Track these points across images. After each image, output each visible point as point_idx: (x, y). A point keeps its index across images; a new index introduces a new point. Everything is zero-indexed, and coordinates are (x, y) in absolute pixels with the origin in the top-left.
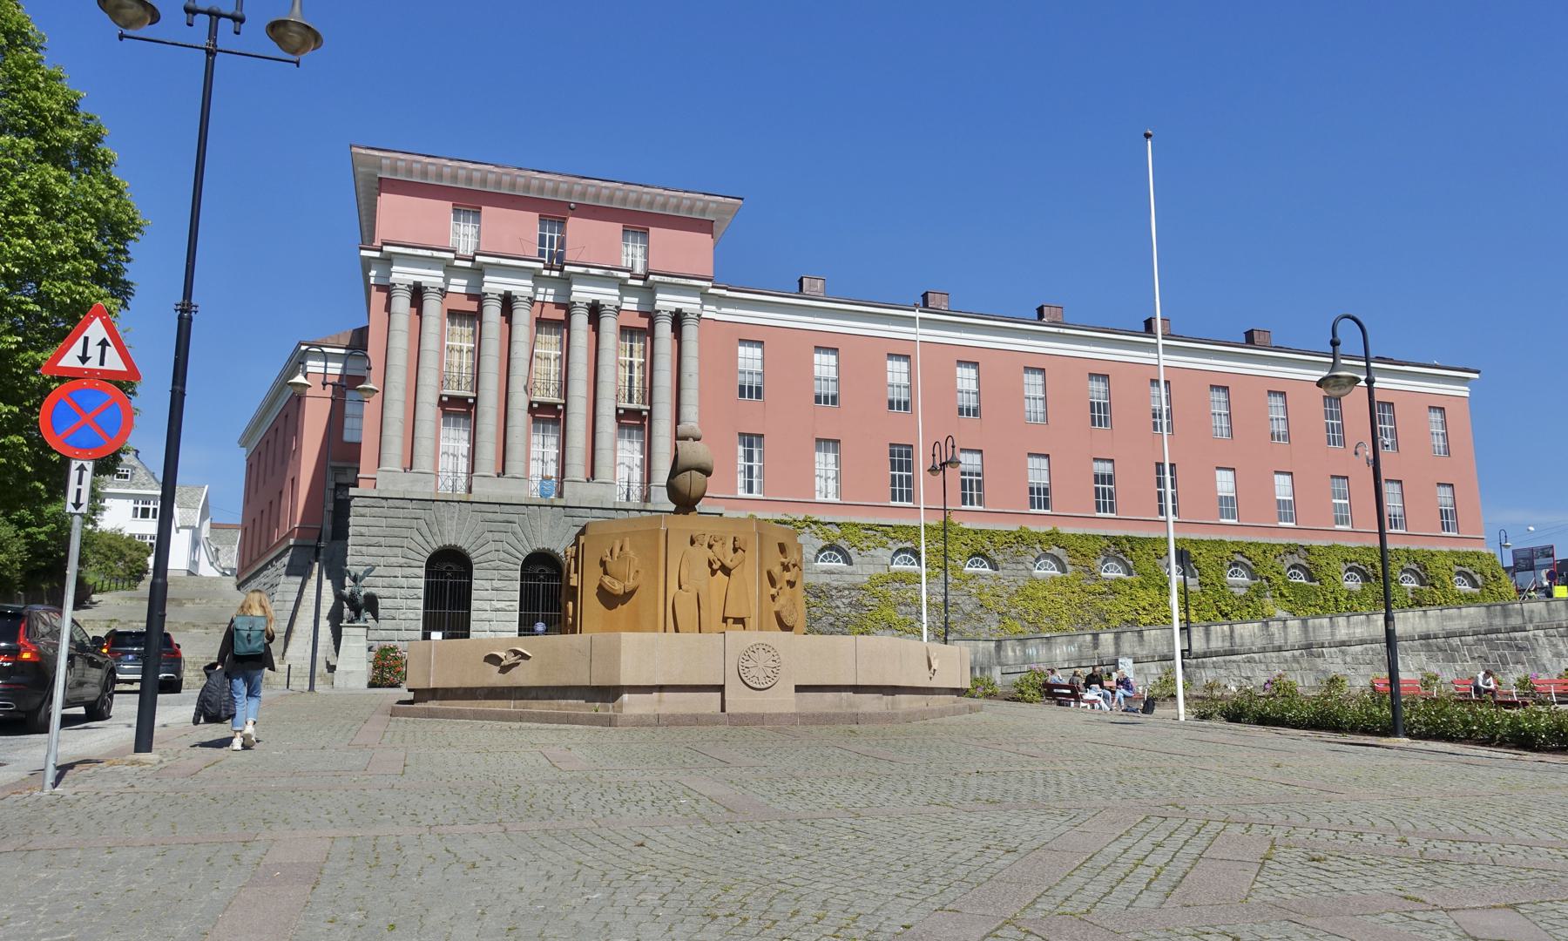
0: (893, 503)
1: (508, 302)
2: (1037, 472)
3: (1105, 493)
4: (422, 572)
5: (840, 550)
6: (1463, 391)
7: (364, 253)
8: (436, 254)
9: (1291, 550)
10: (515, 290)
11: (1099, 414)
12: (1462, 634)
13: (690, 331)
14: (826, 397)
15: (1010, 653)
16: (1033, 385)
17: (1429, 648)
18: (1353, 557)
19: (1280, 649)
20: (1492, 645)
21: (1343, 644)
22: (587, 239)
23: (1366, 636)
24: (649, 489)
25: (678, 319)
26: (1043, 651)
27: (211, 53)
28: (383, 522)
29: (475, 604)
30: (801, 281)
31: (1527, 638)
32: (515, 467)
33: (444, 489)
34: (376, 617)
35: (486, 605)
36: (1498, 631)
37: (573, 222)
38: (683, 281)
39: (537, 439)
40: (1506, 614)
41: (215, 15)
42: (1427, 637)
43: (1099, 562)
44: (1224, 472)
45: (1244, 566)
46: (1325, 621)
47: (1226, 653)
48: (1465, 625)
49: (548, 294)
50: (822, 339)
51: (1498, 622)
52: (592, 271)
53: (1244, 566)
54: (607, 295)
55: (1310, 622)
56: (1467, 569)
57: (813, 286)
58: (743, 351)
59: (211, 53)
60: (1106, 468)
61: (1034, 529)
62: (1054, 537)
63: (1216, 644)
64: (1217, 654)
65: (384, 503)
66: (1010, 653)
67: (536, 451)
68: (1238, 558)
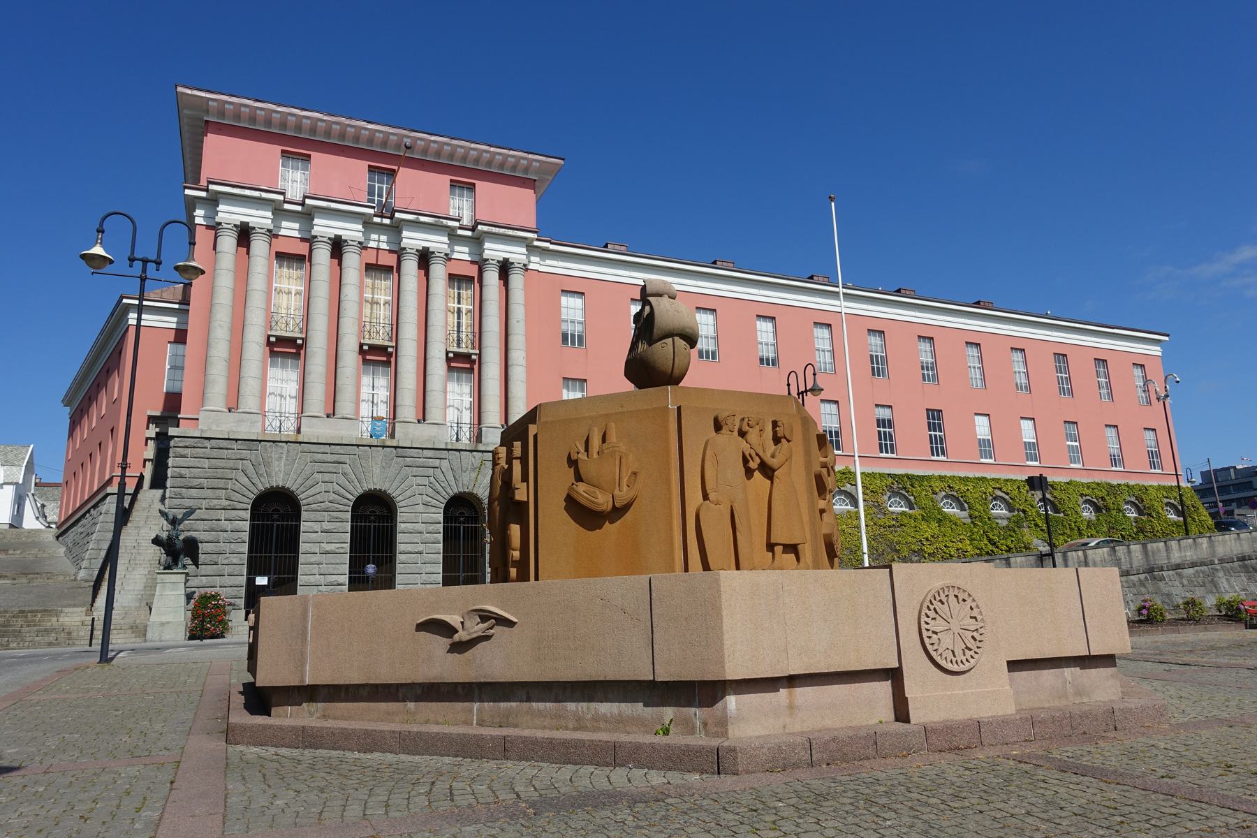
1: (337, 247)
4: (247, 515)
6: (1156, 351)
7: (188, 192)
8: (264, 195)
9: (941, 478)
10: (253, 222)
13: (516, 279)
16: (765, 328)
24: (480, 430)
25: (505, 268)
27: (143, 280)
28: (206, 463)
32: (345, 407)
33: (271, 430)
37: (404, 174)
38: (510, 232)
39: (366, 380)
41: (145, 261)
43: (886, 498)
44: (827, 405)
49: (379, 241)
52: (422, 219)
59: (143, 280)
60: (884, 414)
65: (207, 443)
67: (366, 391)
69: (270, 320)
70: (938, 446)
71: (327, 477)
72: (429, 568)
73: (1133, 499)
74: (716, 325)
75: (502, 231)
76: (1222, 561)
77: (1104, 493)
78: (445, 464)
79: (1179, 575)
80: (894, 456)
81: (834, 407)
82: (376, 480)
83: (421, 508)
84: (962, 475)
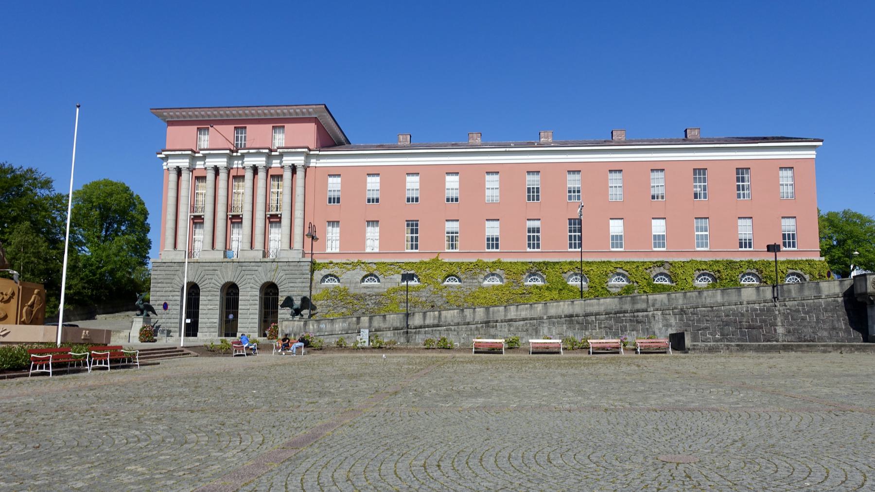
0: (487, 250)
2: (492, 229)
3: (534, 238)
5: (376, 277)
6: (812, 154)
8: (184, 153)
9: (662, 264)
10: (257, 163)
11: (533, 194)
12: (597, 314)
13: (300, 174)
14: (413, 199)
15: (311, 327)
16: (492, 182)
17: (571, 322)
18: (704, 267)
19: (468, 324)
20: (618, 320)
21: (511, 320)
22: (256, 134)
23: (529, 316)
26: (329, 326)
28: (163, 273)
29: (201, 307)
30: (686, 131)
31: (647, 316)
34: (155, 313)
35: (205, 307)
36: (625, 312)
37: (249, 127)
38: (293, 150)
40: (634, 301)
42: (571, 316)
43: (524, 277)
44: (787, 220)
45: (624, 276)
46: (502, 309)
47: (434, 326)
48: (602, 309)
50: (361, 170)
51: (628, 307)
52: (251, 151)
53: (624, 276)
54: (260, 161)
55: (491, 309)
56: (799, 271)
57: (618, 136)
58: (331, 180)
61: (486, 260)
62: (498, 264)
63: (429, 321)
64: (428, 326)
66: (311, 327)
68: (619, 271)
69: (267, 207)
70: (577, 241)
71: (210, 277)
72: (252, 316)
73: (754, 271)
74: (793, 178)
75: (184, 153)
76: (550, 318)
77: (721, 268)
78: (260, 269)
79: (510, 326)
80: (751, 249)
81: (750, 220)
82: (229, 278)
83: (249, 289)
84: (569, 260)
